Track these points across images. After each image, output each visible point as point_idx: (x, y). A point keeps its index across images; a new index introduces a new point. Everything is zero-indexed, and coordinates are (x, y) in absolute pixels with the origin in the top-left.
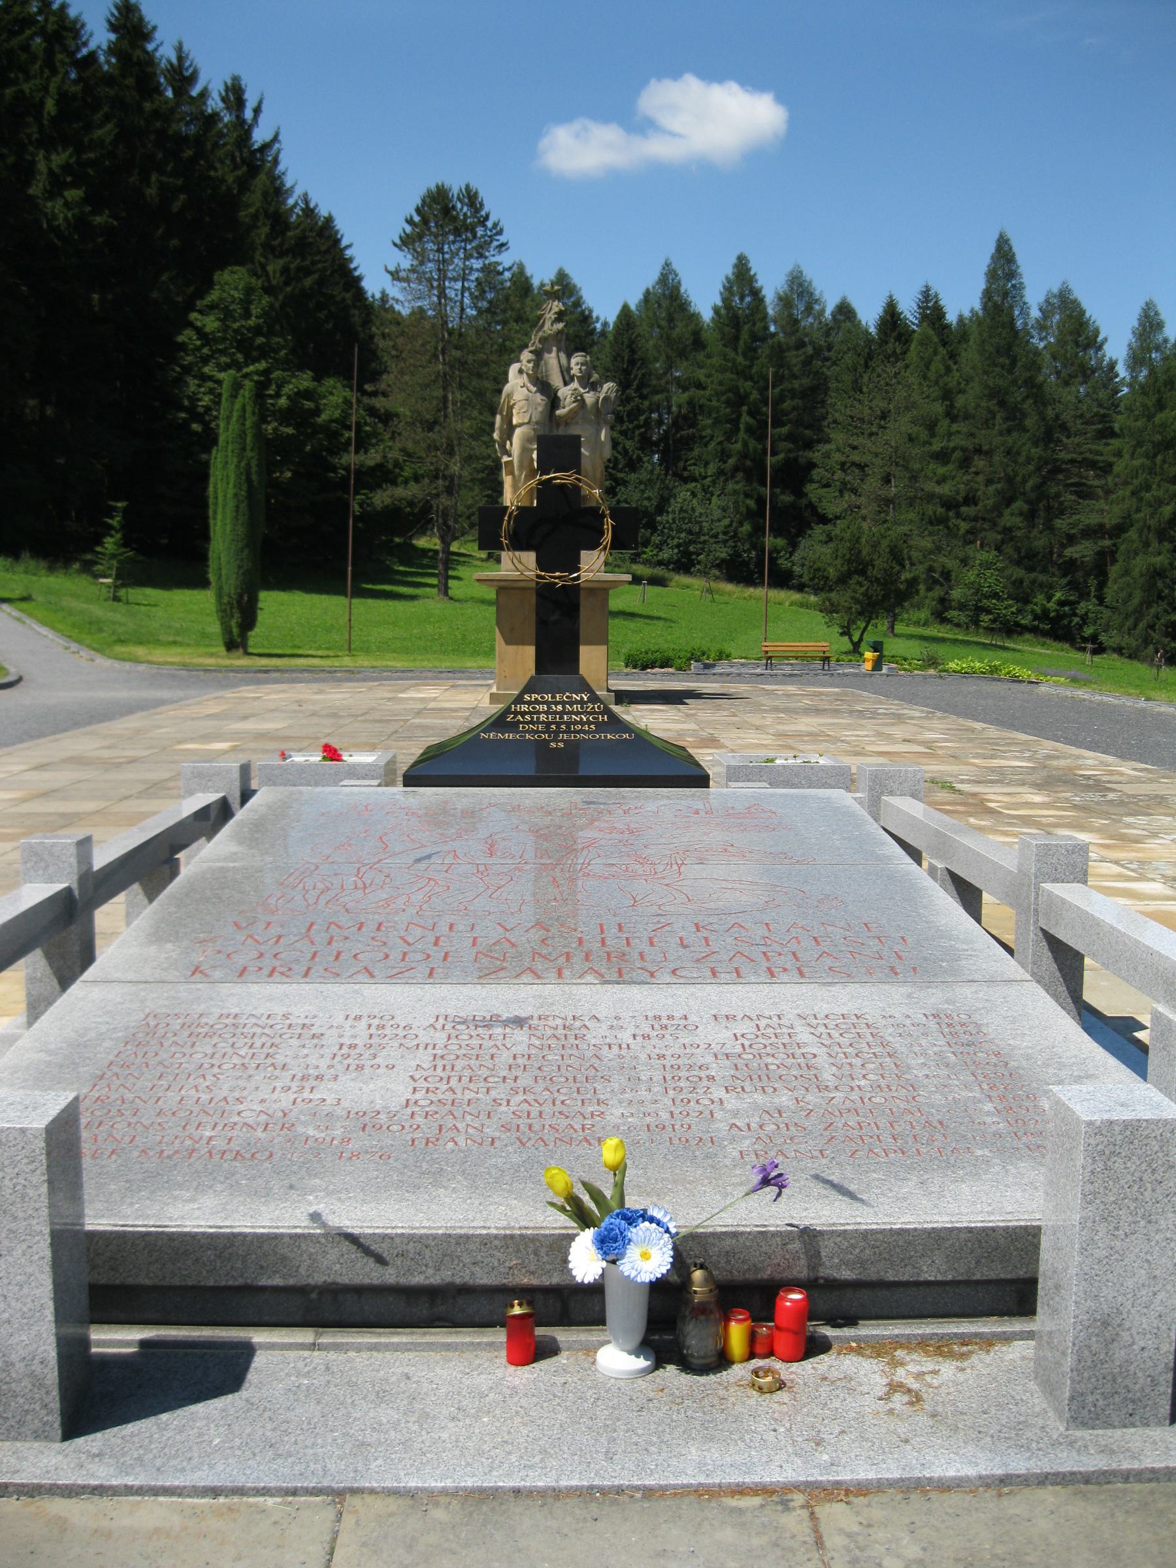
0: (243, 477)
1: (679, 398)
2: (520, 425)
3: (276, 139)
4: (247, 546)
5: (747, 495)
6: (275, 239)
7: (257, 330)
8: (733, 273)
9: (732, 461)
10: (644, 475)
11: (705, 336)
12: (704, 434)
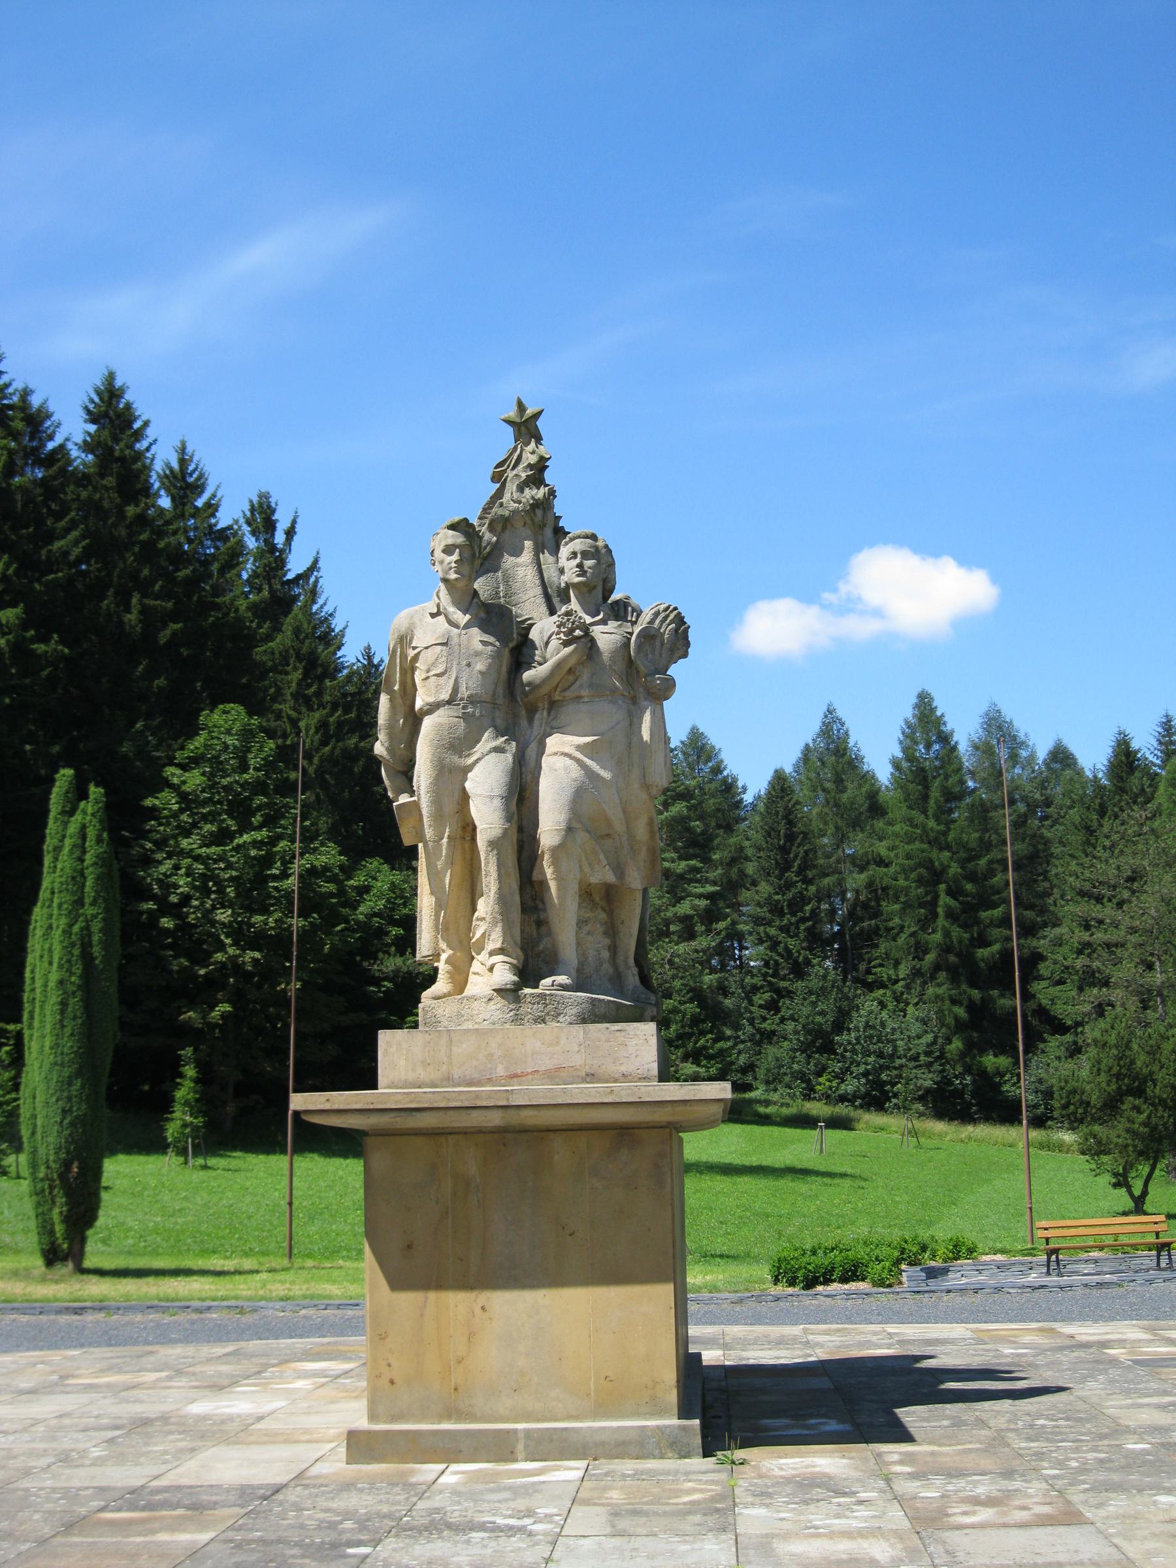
0: (76, 952)
1: (856, 880)
2: (432, 708)
3: (314, 567)
4: (79, 1073)
5: (954, 1002)
6: (309, 686)
7: (259, 787)
8: (914, 716)
9: (930, 957)
10: (814, 983)
11: (883, 797)
12: (891, 924)
